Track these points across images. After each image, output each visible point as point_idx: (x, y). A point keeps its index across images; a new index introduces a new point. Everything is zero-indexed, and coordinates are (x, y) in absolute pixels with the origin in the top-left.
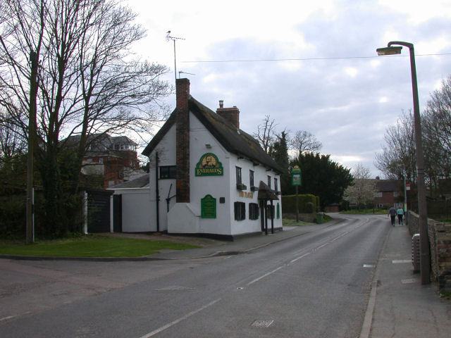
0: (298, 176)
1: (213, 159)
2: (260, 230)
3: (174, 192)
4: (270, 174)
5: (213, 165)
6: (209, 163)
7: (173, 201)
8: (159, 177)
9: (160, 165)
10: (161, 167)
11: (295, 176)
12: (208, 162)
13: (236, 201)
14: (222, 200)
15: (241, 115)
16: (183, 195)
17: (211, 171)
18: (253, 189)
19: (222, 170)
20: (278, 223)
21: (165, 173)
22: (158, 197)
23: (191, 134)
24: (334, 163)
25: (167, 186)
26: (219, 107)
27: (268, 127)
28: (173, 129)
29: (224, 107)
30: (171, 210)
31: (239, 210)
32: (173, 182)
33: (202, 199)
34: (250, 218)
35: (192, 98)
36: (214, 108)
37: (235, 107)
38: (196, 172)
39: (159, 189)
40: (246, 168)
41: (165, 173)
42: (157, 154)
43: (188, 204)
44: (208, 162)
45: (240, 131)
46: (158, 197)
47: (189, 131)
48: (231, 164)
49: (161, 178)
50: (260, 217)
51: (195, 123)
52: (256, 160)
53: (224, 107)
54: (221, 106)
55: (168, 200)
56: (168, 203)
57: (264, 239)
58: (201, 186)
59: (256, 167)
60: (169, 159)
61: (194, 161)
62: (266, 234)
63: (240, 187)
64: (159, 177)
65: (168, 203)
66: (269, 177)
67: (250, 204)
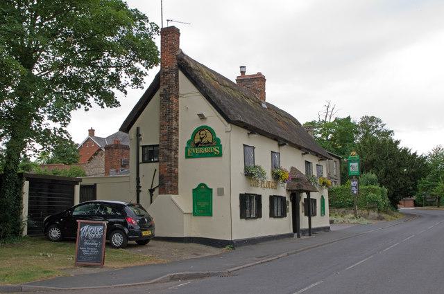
0: (356, 164)
1: (209, 134)
2: (291, 231)
3: (156, 183)
4: (309, 158)
5: (209, 142)
6: (204, 140)
7: (156, 192)
8: (141, 161)
9: (142, 144)
10: (143, 147)
11: (351, 164)
12: (201, 139)
13: (243, 192)
14: (221, 192)
15: (181, 38)
16: (168, 183)
17: (206, 150)
18: (276, 177)
19: (221, 150)
20: (319, 221)
21: (150, 154)
22: (138, 187)
23: (182, 102)
24: (405, 151)
25: (150, 172)
26: (240, 74)
27: (329, 113)
28: (156, 97)
29: (246, 74)
30: (154, 202)
31: (249, 205)
32: (156, 166)
33: (194, 190)
34: (272, 215)
35: (182, 53)
36: (232, 75)
37: (259, 74)
38: (187, 153)
39: (140, 176)
40: (264, 152)
41: (150, 154)
42: (138, 129)
43: (173, 197)
44: (201, 139)
45: (267, 104)
46: (138, 187)
47: (177, 97)
48: (233, 141)
49: (144, 162)
50: (290, 214)
51: (184, 83)
52: (282, 139)
53: (246, 74)
54: (243, 73)
55: (151, 191)
56: (151, 195)
57: (296, 243)
58: (192, 171)
59: (282, 148)
60: (151, 138)
61: (184, 137)
62: (299, 236)
63: (249, 174)
64: (141, 161)
65: (151, 195)
66: (308, 163)
67: (272, 198)
